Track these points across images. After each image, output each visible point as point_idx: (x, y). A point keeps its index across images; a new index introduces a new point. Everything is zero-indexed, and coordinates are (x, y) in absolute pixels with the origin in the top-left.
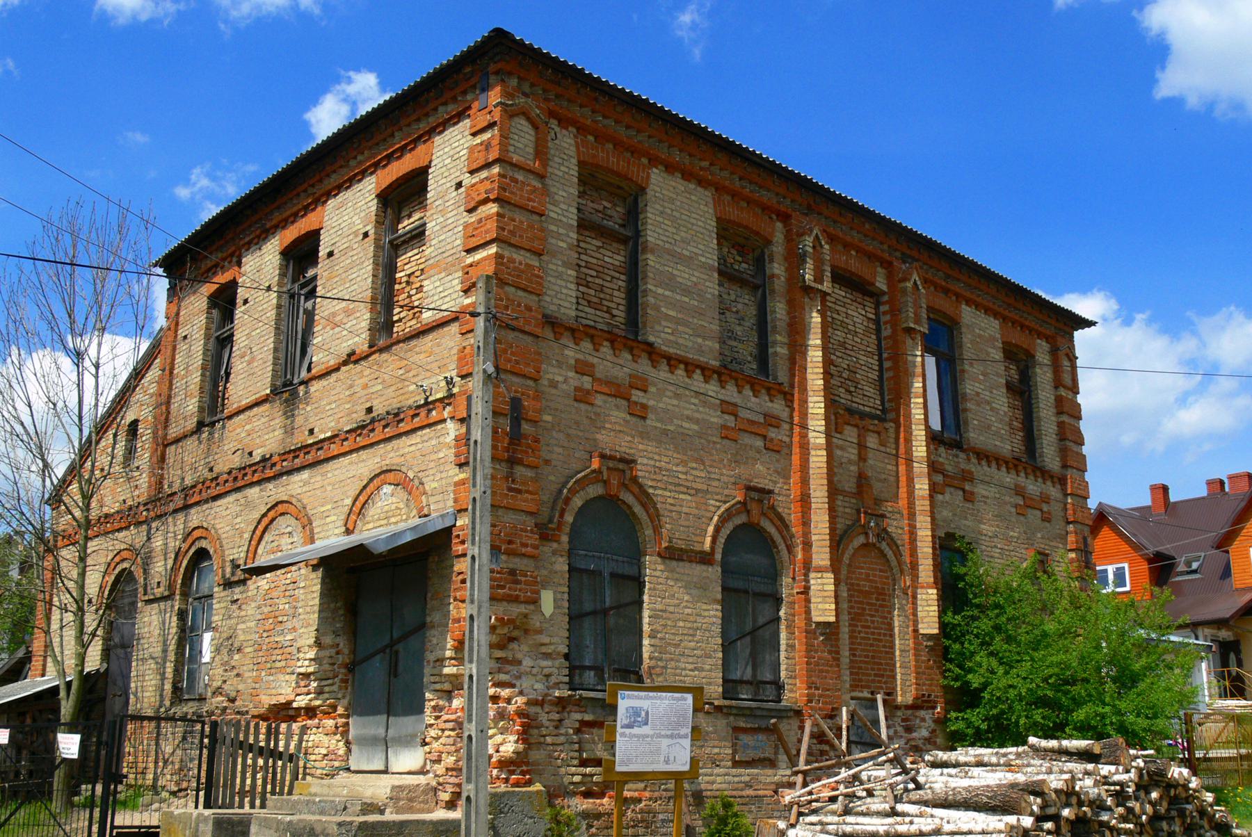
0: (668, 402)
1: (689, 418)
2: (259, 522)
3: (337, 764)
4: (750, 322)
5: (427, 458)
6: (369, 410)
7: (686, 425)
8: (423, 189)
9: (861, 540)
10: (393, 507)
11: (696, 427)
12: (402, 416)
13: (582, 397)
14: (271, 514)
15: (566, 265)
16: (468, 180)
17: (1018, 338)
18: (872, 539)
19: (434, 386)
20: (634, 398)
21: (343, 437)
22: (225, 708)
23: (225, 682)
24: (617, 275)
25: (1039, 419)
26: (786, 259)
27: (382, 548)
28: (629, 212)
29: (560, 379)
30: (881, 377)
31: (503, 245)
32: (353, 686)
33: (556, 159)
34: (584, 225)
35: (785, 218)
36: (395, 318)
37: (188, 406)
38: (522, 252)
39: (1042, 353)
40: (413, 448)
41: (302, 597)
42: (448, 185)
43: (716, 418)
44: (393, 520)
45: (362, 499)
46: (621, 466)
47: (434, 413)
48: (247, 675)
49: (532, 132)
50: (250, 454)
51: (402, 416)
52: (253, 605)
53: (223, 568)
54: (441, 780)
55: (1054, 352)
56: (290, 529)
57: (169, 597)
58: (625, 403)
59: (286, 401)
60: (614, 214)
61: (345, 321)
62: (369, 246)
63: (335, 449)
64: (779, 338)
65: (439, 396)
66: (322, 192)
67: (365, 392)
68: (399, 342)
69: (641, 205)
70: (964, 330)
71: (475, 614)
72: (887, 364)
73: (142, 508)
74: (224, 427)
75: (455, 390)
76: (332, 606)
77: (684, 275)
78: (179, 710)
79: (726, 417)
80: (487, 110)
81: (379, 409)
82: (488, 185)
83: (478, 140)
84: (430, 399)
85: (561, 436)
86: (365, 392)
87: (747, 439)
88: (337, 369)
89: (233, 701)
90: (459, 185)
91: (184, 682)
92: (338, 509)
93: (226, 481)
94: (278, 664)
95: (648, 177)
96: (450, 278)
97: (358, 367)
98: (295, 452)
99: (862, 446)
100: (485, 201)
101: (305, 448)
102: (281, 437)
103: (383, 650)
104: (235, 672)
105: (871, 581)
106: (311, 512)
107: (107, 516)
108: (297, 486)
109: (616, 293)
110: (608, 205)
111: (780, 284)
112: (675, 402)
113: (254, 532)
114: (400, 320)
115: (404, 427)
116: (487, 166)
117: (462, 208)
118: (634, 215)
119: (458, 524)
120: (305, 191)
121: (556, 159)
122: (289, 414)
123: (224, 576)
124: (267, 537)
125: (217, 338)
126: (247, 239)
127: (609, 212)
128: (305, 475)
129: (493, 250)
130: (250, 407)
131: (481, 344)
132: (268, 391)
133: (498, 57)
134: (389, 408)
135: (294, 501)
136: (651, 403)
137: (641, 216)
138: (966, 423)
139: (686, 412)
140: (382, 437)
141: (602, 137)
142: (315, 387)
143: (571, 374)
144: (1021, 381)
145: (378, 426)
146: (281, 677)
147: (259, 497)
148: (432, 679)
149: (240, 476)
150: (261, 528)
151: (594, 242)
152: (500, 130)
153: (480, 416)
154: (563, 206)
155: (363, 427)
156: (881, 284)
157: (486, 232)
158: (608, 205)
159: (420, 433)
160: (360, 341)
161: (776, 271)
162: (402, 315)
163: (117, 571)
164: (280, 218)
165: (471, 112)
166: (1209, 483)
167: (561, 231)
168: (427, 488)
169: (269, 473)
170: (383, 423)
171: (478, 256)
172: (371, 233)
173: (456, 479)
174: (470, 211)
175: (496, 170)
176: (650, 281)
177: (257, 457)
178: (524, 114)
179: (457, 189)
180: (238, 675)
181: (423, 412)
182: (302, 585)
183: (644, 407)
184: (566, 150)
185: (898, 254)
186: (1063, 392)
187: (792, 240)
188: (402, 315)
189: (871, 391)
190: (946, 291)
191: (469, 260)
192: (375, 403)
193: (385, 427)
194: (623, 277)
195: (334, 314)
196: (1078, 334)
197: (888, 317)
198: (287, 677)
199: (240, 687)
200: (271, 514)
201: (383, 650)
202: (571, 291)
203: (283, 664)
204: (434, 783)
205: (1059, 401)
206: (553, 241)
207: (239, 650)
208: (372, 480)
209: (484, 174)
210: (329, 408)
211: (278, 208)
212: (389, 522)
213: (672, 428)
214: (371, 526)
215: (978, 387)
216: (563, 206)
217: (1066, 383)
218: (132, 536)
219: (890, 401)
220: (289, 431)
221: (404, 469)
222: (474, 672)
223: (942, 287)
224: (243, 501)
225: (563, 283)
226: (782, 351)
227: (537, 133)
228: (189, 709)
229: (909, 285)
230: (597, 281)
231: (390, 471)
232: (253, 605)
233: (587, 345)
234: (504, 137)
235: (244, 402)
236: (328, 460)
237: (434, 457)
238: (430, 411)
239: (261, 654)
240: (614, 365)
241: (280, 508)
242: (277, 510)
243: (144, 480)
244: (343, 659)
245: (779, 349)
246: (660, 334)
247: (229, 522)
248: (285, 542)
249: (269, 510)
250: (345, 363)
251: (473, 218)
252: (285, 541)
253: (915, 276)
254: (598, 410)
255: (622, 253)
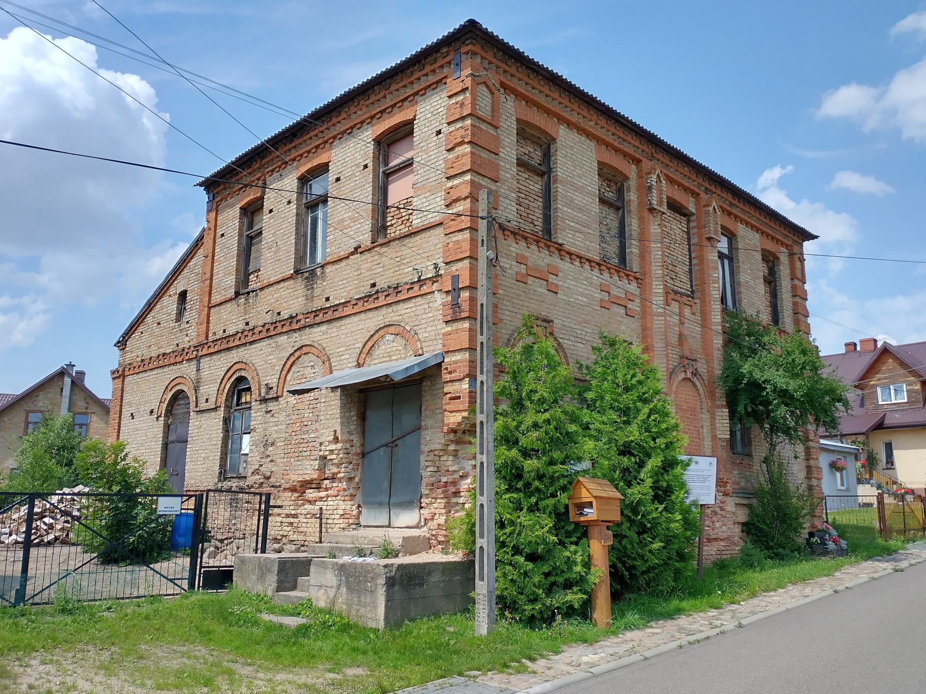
0: (570, 283)
1: (582, 294)
2: (288, 359)
3: (351, 521)
4: (614, 231)
5: (420, 317)
6: (373, 285)
7: (580, 298)
8: (411, 133)
9: (682, 376)
10: (394, 349)
11: (586, 300)
12: (400, 289)
13: (521, 280)
14: (297, 354)
15: (510, 189)
16: (445, 129)
17: (771, 246)
18: (689, 375)
19: (424, 270)
20: (550, 280)
21: (354, 302)
22: (262, 483)
23: (261, 465)
24: (537, 198)
25: (782, 299)
26: (637, 190)
27: (397, 378)
28: (544, 155)
29: (508, 266)
30: (690, 270)
31: (475, 174)
32: (362, 468)
33: (504, 116)
34: (521, 163)
35: (637, 162)
36: (389, 224)
37: (226, 281)
38: (486, 179)
39: (784, 258)
40: (409, 310)
41: (323, 409)
42: (430, 132)
43: (598, 295)
44: (394, 358)
45: (370, 344)
46: (545, 324)
47: (425, 287)
48: (279, 461)
49: (490, 96)
50: (279, 314)
51: (400, 289)
52: (284, 414)
53: (260, 389)
54: (434, 533)
55: (791, 255)
56: (312, 364)
57: (215, 409)
58: (545, 283)
59: (307, 278)
60: (535, 156)
61: (352, 225)
62: (369, 174)
63: (348, 310)
64: (634, 242)
65: (429, 276)
66: (330, 135)
67: (370, 273)
68: (394, 240)
69: (552, 151)
70: (739, 240)
71: (485, 421)
72: (694, 262)
73: (192, 349)
74: (257, 295)
75: (441, 272)
76: (347, 414)
77: (578, 199)
78: (226, 484)
79: (604, 293)
80: (460, 79)
81: (382, 284)
82: (462, 132)
83: (453, 101)
84: (422, 278)
85: (508, 303)
86: (370, 273)
87: (616, 309)
88: (347, 257)
89: (268, 478)
90: (439, 132)
91: (228, 467)
92: (352, 353)
93: (260, 332)
94: (304, 454)
95: (558, 132)
96: (434, 196)
97: (364, 257)
98: (316, 313)
99: (681, 315)
100: (462, 143)
101: (324, 310)
102: (304, 302)
103: (386, 445)
104: (269, 459)
105: (688, 403)
106: (329, 353)
107: (164, 354)
108: (315, 335)
109: (537, 210)
110: (532, 150)
111: (634, 206)
112: (574, 283)
113: (284, 365)
114: (392, 225)
115: (401, 297)
116: (463, 118)
117: (443, 148)
118: (547, 156)
119: (446, 360)
120: (316, 135)
121: (504, 116)
122: (310, 286)
123: (260, 395)
124: (293, 369)
125: (248, 236)
126: (271, 168)
127: (532, 155)
128: (324, 328)
129: (468, 177)
130: (278, 282)
131: (485, 238)
132: (292, 272)
133: (469, 41)
134: (389, 284)
135: (316, 345)
136: (560, 283)
137: (553, 158)
138: (740, 301)
139: (580, 290)
140: (385, 303)
141: (530, 102)
142: (329, 269)
143: (514, 263)
144: (769, 275)
145: (382, 297)
146: (307, 462)
147: (287, 343)
148: (427, 464)
149: (272, 329)
150: (289, 363)
151: (523, 175)
152: (472, 94)
153: (485, 287)
154: (508, 149)
155: (370, 296)
156: (692, 208)
157: (463, 165)
158: (532, 150)
159: (413, 301)
160: (365, 238)
161: (632, 198)
162: (393, 222)
163: (173, 392)
164: (297, 154)
165: (448, 81)
166: (847, 345)
167: (507, 166)
168: (420, 337)
169: (295, 326)
170: (385, 293)
171: (456, 182)
172: (370, 165)
173: (443, 331)
174: (449, 150)
175: (468, 122)
176: (559, 202)
177: (285, 315)
178: (484, 83)
179: (437, 135)
180: (272, 461)
181: (416, 287)
182: (323, 400)
183: (557, 286)
184: (510, 112)
185: (703, 188)
186: (796, 282)
187: (642, 177)
188: (393, 222)
189: (685, 279)
190: (730, 214)
191: (450, 184)
192: (377, 280)
193: (386, 296)
194: (541, 200)
195: (343, 221)
196: (806, 244)
197: (696, 230)
198: (312, 462)
199: (274, 469)
200: (297, 354)
201: (386, 445)
202: (513, 207)
203: (308, 453)
204: (428, 535)
205: (794, 288)
206: (502, 173)
207: (273, 444)
208: (377, 331)
209: (459, 125)
210: (340, 284)
211: (295, 147)
212: (392, 361)
213: (572, 300)
214: (377, 361)
215: (747, 278)
216: (509, 149)
217: (798, 277)
218: (188, 369)
219: (696, 285)
220: (310, 298)
221: (402, 324)
222: (485, 460)
223: (728, 211)
224: (274, 345)
225: (508, 202)
226: (635, 251)
227: (493, 98)
228: (234, 484)
229: (711, 209)
230: (526, 201)
231: (392, 325)
232: (284, 414)
233: (523, 243)
234: (474, 99)
235: (272, 280)
236: (341, 318)
237: (424, 316)
238: (421, 286)
239: (290, 447)
240: (539, 258)
241: (305, 350)
242: (300, 351)
243: (193, 332)
244: (357, 449)
245: (634, 250)
246: (565, 237)
247: (264, 361)
248: (308, 373)
249: (295, 351)
250: (352, 254)
251: (451, 156)
252: (309, 371)
253: (714, 204)
254: (530, 287)
255: (540, 183)
